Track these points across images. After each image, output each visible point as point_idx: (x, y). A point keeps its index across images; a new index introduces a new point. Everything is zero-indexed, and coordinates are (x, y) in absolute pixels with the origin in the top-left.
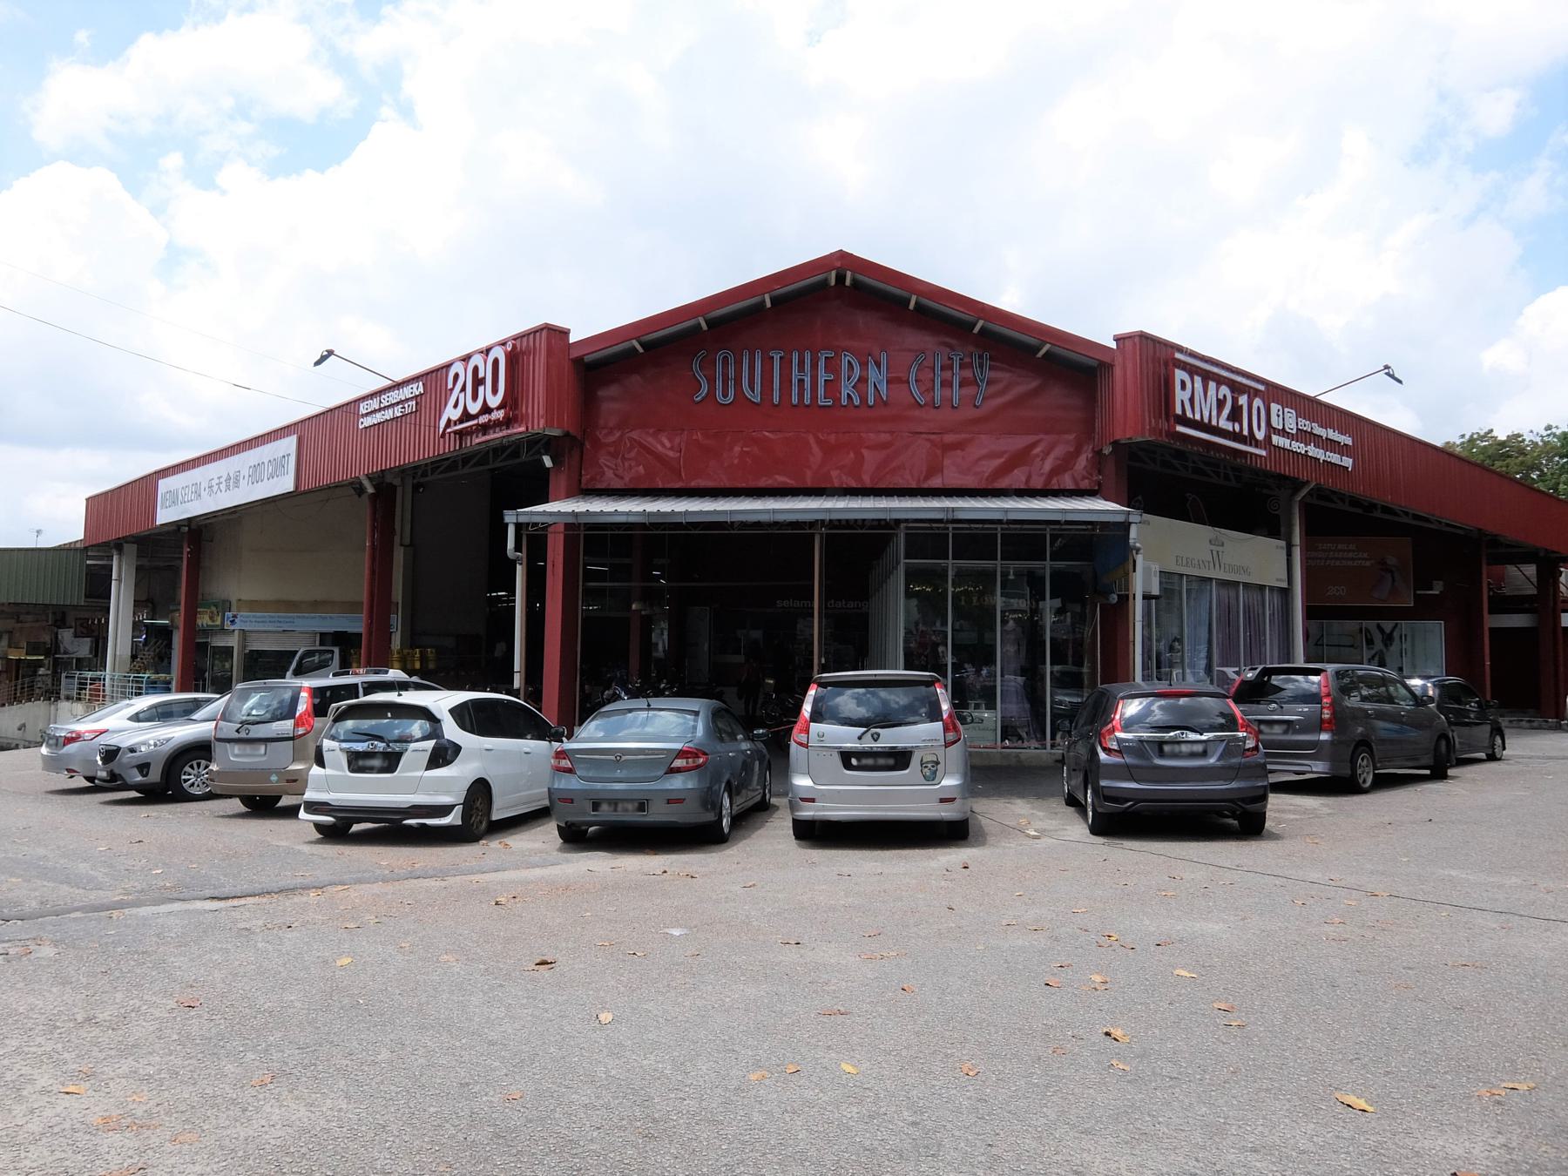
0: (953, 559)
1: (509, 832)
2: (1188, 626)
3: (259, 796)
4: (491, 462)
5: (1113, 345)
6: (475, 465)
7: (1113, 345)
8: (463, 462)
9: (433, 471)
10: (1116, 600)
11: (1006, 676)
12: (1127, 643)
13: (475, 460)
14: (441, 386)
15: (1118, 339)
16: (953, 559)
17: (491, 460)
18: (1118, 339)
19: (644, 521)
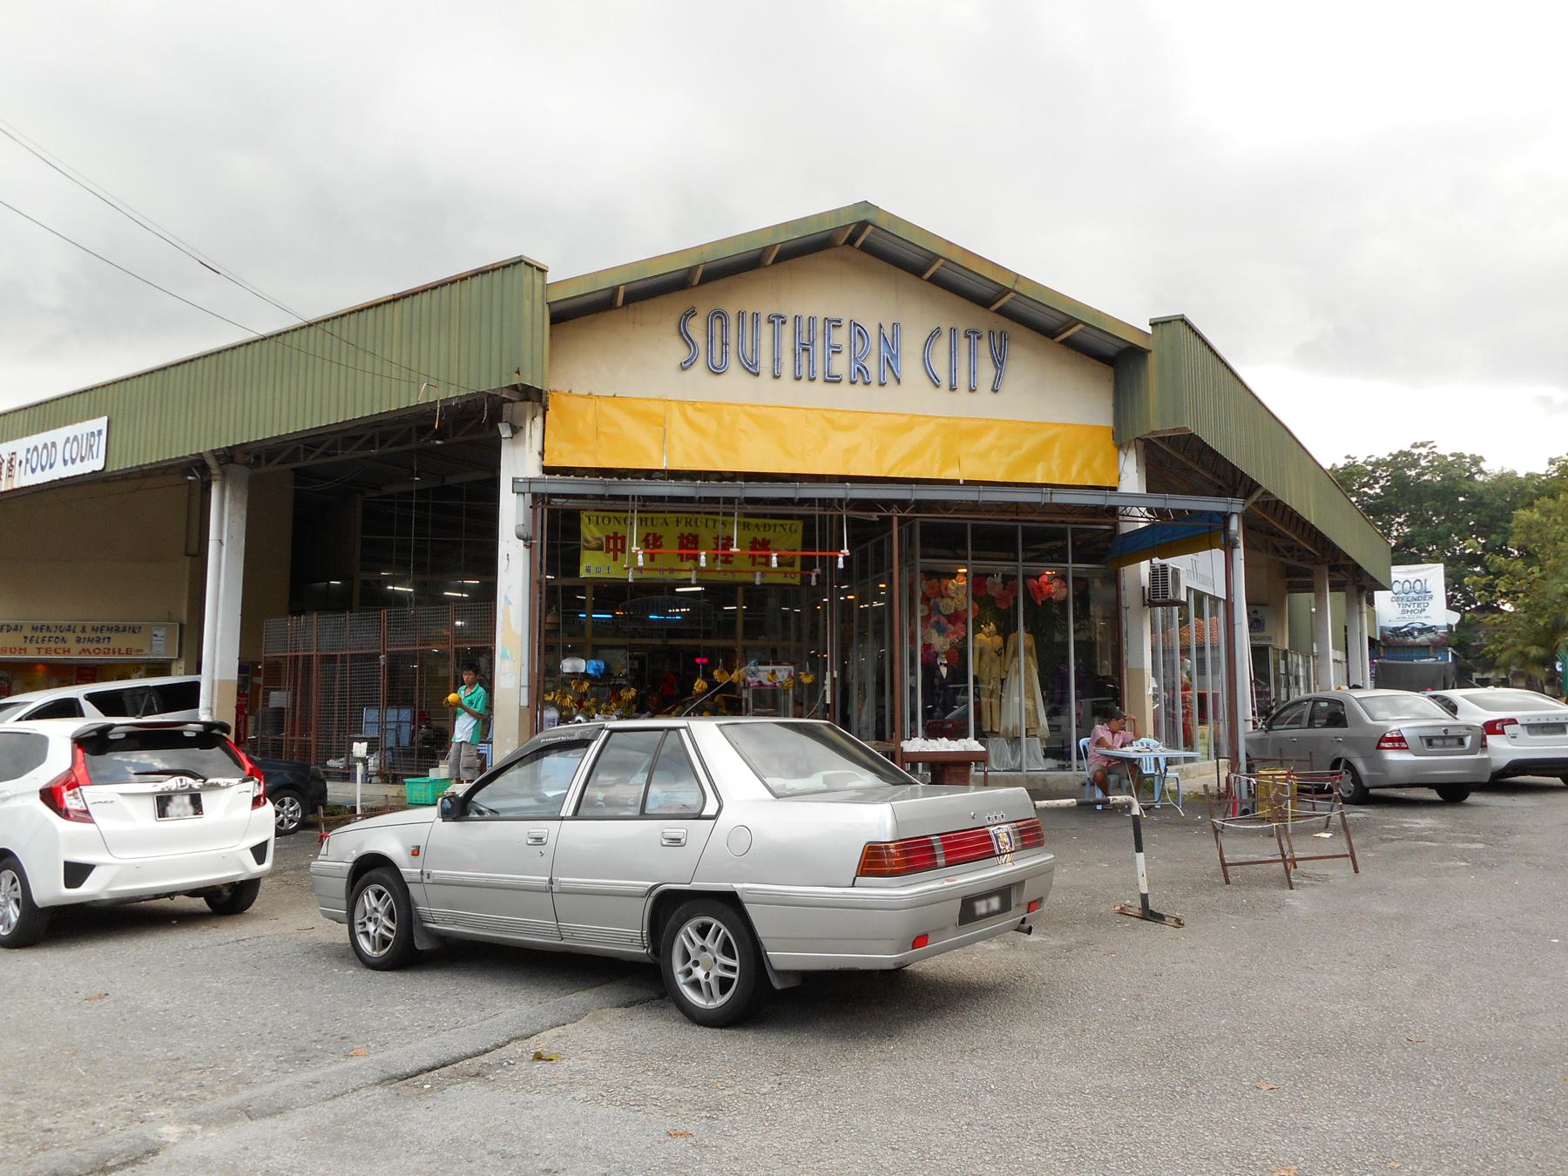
0: (1073, 562)
1: (50, 946)
2: (1303, 823)
3: (1447, 592)
4: (302, 459)
5: (1149, 330)
6: (395, 444)
7: (1149, 330)
8: (305, 450)
9: (308, 452)
10: (1557, 667)
11: (548, 879)
12: (1250, 824)
13: (282, 456)
14: (258, 402)
15: (1153, 324)
16: (1073, 562)
17: (302, 456)
18: (1153, 324)
19: (603, 493)
